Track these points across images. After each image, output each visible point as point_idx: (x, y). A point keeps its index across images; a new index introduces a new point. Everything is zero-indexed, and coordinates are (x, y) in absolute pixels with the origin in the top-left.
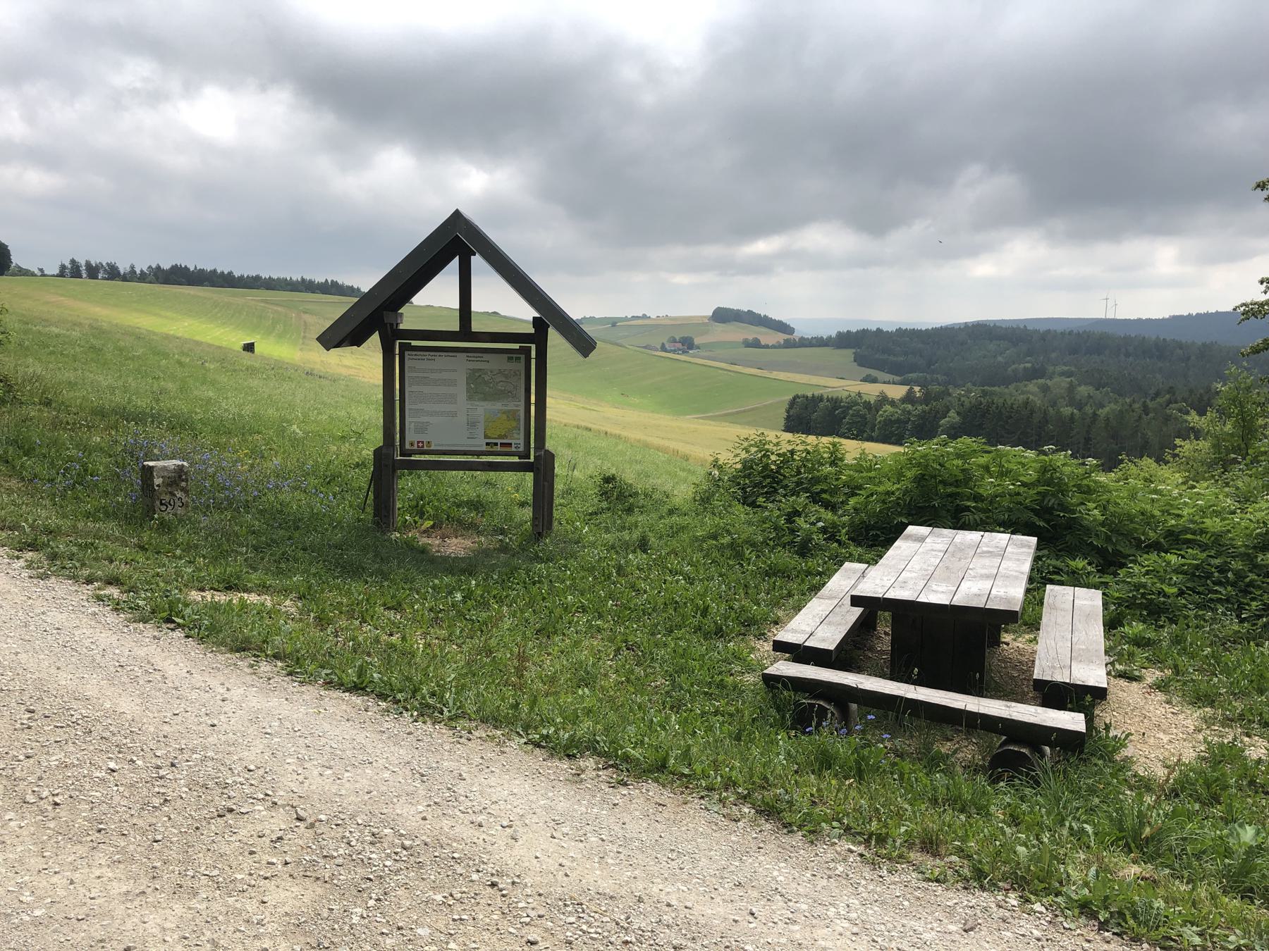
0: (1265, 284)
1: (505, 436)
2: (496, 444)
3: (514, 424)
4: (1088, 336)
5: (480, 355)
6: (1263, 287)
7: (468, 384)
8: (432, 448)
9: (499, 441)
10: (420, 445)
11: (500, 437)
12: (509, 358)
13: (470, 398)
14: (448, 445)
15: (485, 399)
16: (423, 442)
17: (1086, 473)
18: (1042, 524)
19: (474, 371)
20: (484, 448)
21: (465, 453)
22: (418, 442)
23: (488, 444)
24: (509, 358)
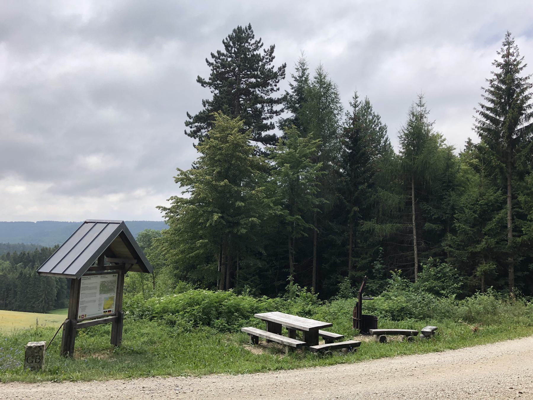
0: (262, 58)
1: (109, 308)
2: (106, 311)
3: (113, 302)
4: (410, 125)
5: (104, 275)
6: (179, 184)
7: (100, 287)
8: (87, 317)
9: (107, 310)
10: (83, 317)
11: (109, 308)
12: (114, 275)
13: (100, 293)
14: (92, 315)
15: (105, 293)
16: (83, 315)
17: (258, 370)
18: (262, 274)
19: (103, 282)
20: (103, 314)
21: (98, 318)
22: (82, 316)
23: (104, 312)
24: (114, 275)
